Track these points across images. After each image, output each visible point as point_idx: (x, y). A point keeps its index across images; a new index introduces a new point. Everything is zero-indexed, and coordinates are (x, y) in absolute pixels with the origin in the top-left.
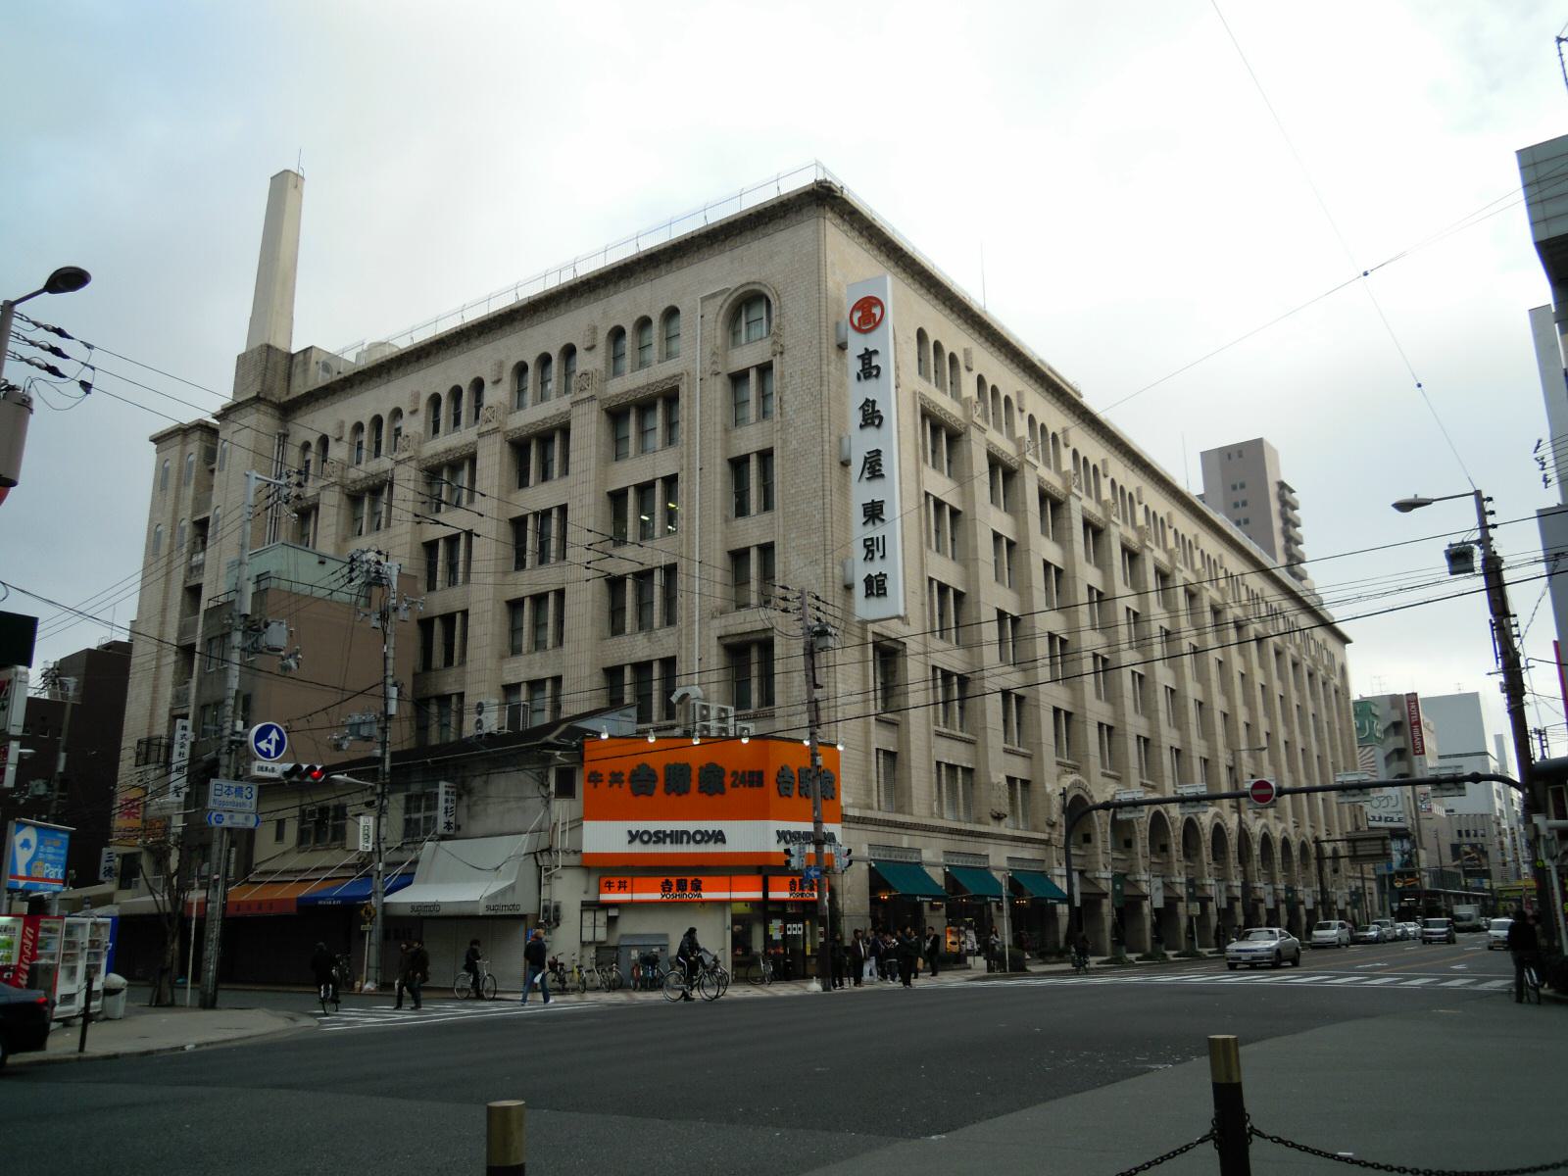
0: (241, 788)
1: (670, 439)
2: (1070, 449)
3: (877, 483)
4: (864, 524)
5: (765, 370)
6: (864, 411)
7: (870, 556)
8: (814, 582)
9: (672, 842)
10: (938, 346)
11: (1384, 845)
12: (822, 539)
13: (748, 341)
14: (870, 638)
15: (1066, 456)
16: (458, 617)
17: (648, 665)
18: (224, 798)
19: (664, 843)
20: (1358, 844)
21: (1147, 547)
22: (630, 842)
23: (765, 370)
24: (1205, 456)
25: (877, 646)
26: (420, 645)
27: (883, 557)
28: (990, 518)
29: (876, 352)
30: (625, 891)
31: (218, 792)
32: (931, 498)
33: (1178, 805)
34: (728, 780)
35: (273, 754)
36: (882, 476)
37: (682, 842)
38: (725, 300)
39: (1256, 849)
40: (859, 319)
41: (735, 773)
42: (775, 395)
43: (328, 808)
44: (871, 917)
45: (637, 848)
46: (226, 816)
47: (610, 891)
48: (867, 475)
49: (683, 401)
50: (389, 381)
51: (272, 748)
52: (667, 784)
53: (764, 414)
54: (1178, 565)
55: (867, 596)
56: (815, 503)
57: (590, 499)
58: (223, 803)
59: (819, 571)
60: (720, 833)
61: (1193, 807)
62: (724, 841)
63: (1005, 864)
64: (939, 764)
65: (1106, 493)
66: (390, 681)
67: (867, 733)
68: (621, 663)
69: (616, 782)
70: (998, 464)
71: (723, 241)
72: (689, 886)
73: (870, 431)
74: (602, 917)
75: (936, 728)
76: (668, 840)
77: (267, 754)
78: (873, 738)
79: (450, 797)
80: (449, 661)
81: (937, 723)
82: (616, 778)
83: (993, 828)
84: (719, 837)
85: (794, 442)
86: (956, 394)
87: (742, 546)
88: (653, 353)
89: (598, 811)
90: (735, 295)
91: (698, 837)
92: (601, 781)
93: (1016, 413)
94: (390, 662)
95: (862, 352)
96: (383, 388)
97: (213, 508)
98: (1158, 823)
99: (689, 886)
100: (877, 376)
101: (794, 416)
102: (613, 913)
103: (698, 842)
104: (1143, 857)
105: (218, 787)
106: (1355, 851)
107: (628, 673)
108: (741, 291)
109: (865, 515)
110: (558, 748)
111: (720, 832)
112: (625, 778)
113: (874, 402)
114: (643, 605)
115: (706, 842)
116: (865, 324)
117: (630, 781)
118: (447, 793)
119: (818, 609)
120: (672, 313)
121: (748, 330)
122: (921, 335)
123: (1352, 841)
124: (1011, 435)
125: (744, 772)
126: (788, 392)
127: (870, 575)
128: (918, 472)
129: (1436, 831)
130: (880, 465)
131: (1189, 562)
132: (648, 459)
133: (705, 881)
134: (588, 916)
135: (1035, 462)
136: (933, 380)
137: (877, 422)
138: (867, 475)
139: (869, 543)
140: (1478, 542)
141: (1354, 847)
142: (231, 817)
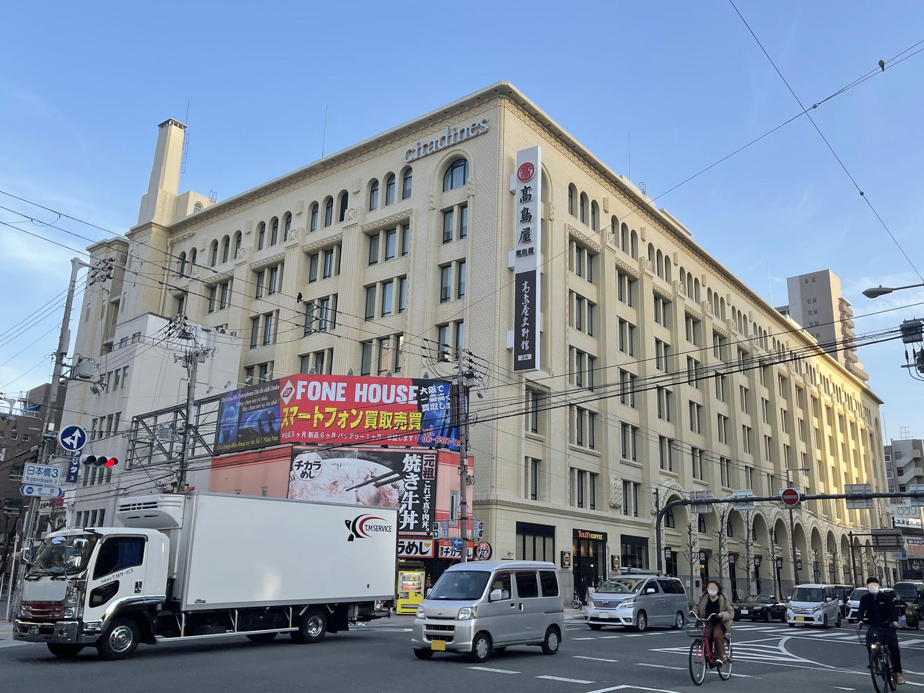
0: (49, 470)
2: (706, 288)
5: (463, 206)
10: (583, 196)
11: (898, 540)
15: (605, 222)
16: (269, 364)
18: (35, 476)
20: (879, 538)
25: (528, 388)
28: (653, 330)
31: (30, 472)
35: (75, 447)
46: (35, 488)
51: (75, 443)
54: (792, 372)
58: (34, 480)
61: (744, 505)
64: (572, 469)
67: (519, 445)
70: (716, 335)
77: (71, 447)
78: (523, 449)
81: (571, 441)
93: (602, 212)
97: (123, 293)
105: (30, 468)
106: (877, 543)
119: (471, 361)
122: (572, 188)
123: (875, 535)
124: (723, 319)
128: (565, 276)
131: (743, 329)
135: (683, 296)
136: (720, 318)
141: (877, 540)
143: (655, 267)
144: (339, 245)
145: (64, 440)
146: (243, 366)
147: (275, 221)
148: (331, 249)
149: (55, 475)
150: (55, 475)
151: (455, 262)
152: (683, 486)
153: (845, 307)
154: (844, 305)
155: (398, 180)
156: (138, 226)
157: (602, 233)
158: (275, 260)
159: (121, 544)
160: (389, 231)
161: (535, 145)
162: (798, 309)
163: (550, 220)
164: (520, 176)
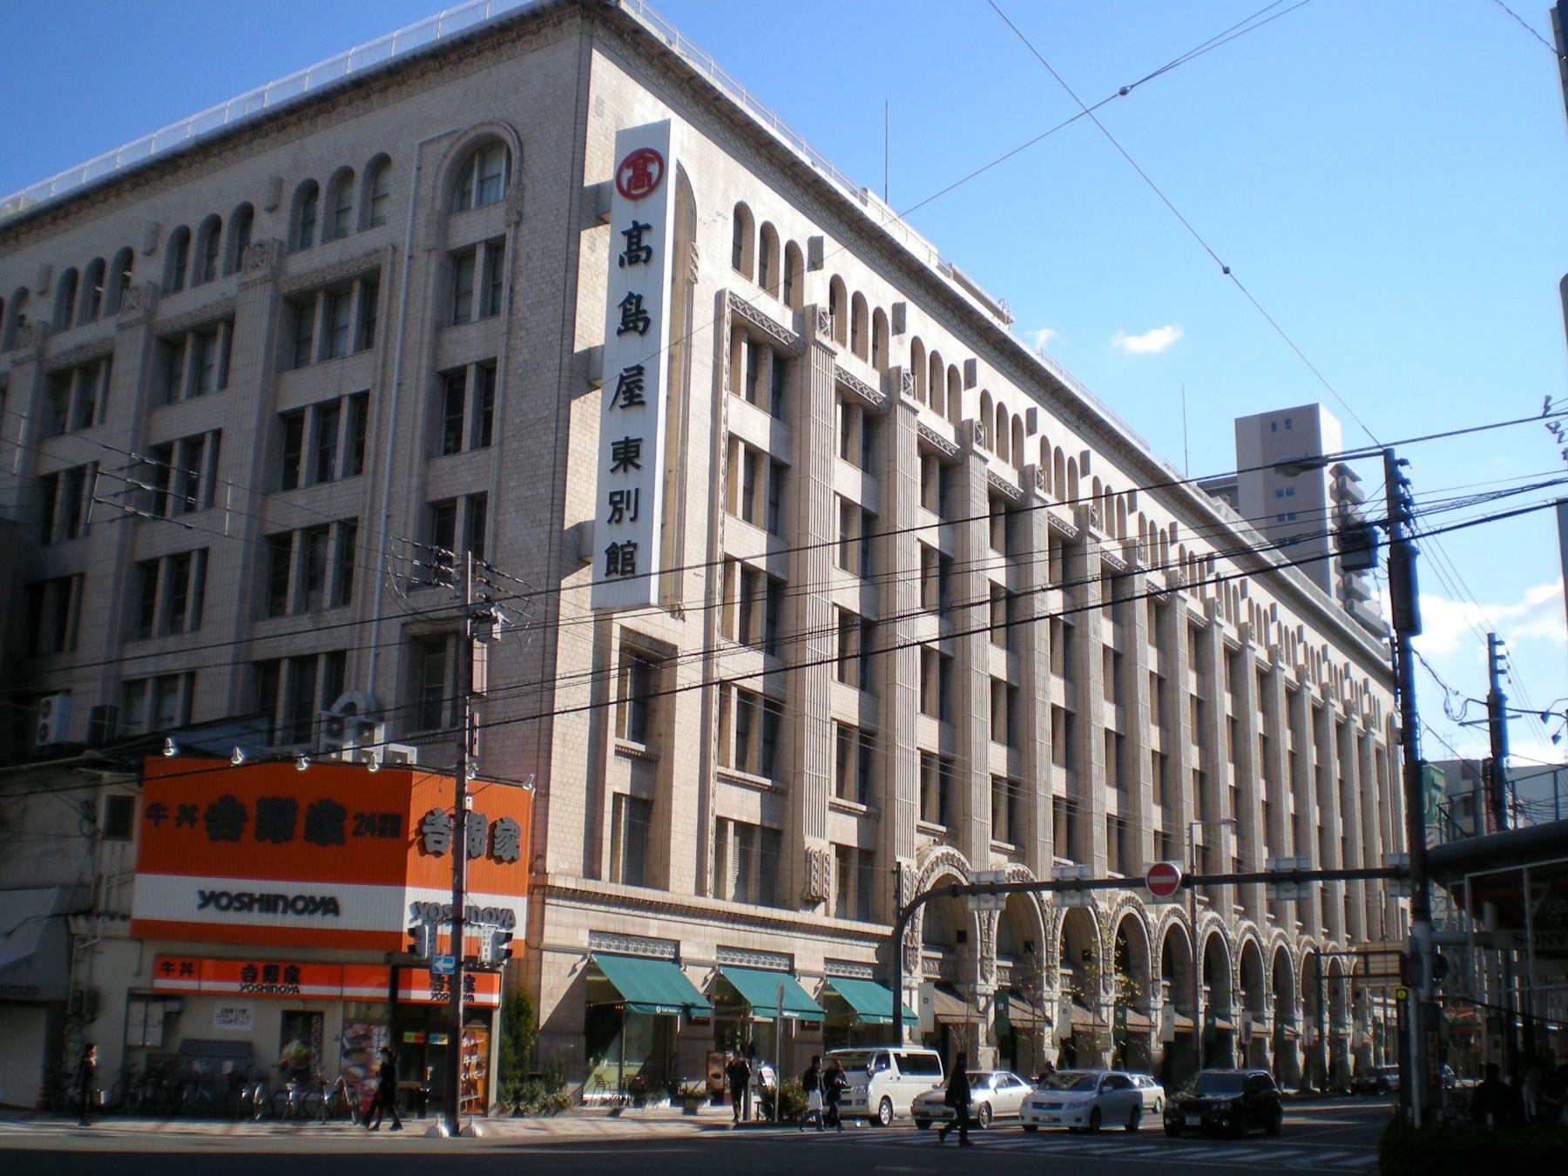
1: (366, 341)
3: (634, 412)
4: (612, 471)
6: (625, 310)
7: (617, 517)
12: (550, 489)
16: (75, 581)
17: (312, 659)
21: (1091, 535)
23: (495, 248)
24: (1242, 424)
27: (633, 519)
29: (648, 227)
32: (741, 446)
34: (350, 825)
36: (642, 403)
38: (451, 147)
39: (1267, 974)
40: (629, 181)
42: (504, 283)
43: (512, 926)
44: (586, 1033)
45: (212, 916)
47: (167, 976)
48: (622, 402)
49: (384, 290)
53: (491, 309)
56: (544, 439)
57: (251, 423)
59: (544, 536)
63: (820, 967)
65: (1032, 455)
68: (274, 656)
72: (282, 974)
73: (632, 338)
74: (157, 1011)
75: (723, 770)
76: (256, 907)
80: (59, 646)
82: (187, 814)
85: (525, 351)
87: (447, 496)
89: (155, 861)
90: (465, 140)
91: (300, 905)
92: (166, 817)
98: (1078, 929)
99: (282, 974)
100: (647, 261)
101: (527, 314)
102: (173, 1006)
103: (300, 912)
107: (284, 668)
108: (472, 134)
109: (614, 459)
113: (639, 298)
114: (312, 580)
116: (636, 188)
120: (381, 163)
126: (522, 280)
127: (614, 545)
129: (494, 826)
130: (641, 388)
132: (334, 366)
134: (138, 1008)
137: (641, 325)
139: (617, 498)
144: (230, 321)
148: (94, 366)
152: (968, 856)
153: (1349, 485)
154: (1348, 479)
155: (356, 191)
159: (300, 1020)
160: (336, 293)
162: (1253, 486)
164: (625, 184)
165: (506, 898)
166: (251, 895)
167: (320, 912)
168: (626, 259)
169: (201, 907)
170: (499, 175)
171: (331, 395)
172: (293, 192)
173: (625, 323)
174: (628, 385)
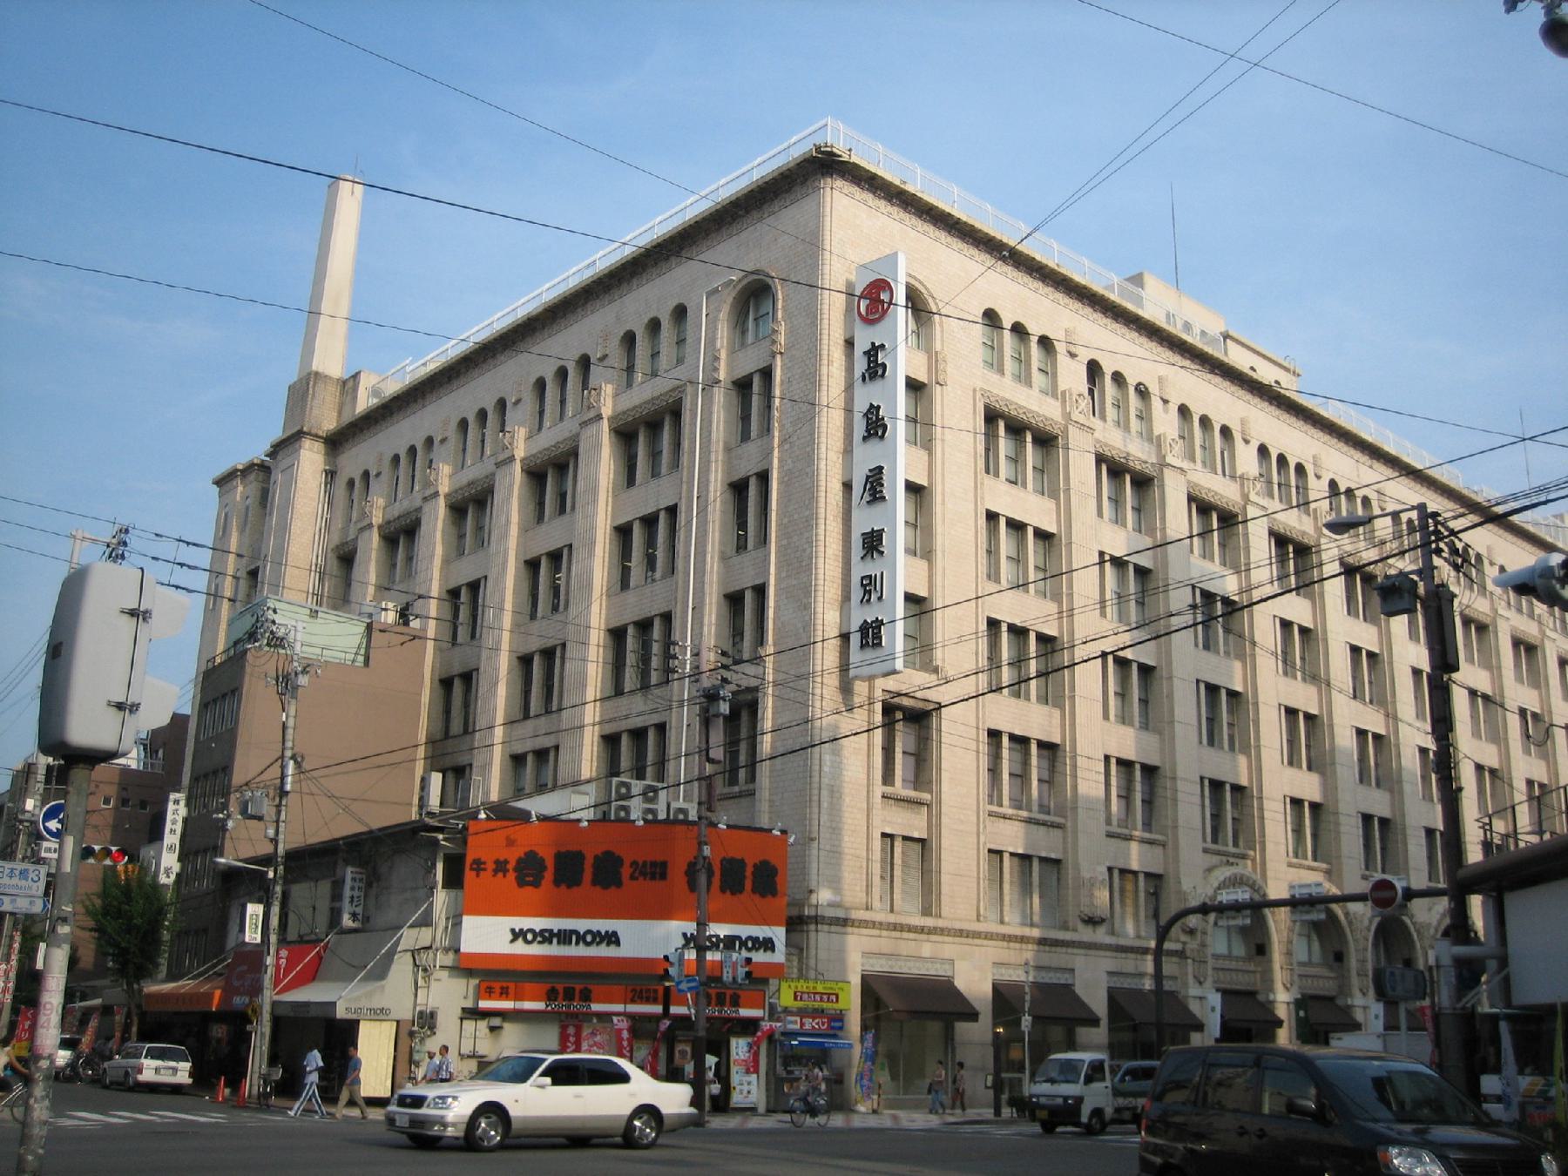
3: (879, 507)
7: (866, 598)
8: (801, 631)
9: (559, 943)
13: (757, 339)
14: (879, 694)
19: (551, 942)
22: (512, 941)
26: (441, 709)
30: (507, 998)
33: (1288, 908)
34: (626, 871)
37: (570, 943)
41: (634, 864)
45: (520, 948)
47: (490, 998)
50: (424, 406)
52: (595, 875)
55: (862, 646)
60: (615, 934)
61: (1308, 912)
62: (618, 943)
66: (288, 753)
69: (500, 871)
71: (730, 224)
73: (874, 444)
79: (356, 885)
82: (501, 867)
83: (1086, 934)
84: (612, 939)
86: (1053, 391)
87: (737, 588)
88: (664, 361)
90: (740, 286)
91: (589, 938)
92: (485, 870)
94: (290, 732)
95: (869, 346)
96: (419, 414)
100: (883, 375)
103: (588, 944)
104: (1359, 975)
109: (864, 548)
110: (440, 830)
111: (615, 934)
112: (510, 867)
115: (598, 944)
117: (515, 870)
118: (354, 879)
121: (757, 325)
122: (991, 317)
125: (645, 862)
133: (596, 989)
134: (469, 1025)
138: (867, 497)
140: (1419, 572)
142: (13, 901)
143: (1215, 461)
144: (676, 412)
145: (47, 824)
146: (437, 678)
147: (562, 374)
149: (36, 879)
150: (36, 879)
151: (638, 521)
156: (284, 437)
157: (1063, 398)
158: (563, 448)
161: (888, 252)
163: (938, 383)
165: (766, 928)
166: (551, 931)
167: (762, 951)
168: (867, 375)
169: (512, 941)
170: (768, 313)
171: (650, 510)
172: (668, 317)
173: (868, 430)
174: (872, 483)
